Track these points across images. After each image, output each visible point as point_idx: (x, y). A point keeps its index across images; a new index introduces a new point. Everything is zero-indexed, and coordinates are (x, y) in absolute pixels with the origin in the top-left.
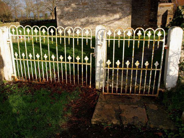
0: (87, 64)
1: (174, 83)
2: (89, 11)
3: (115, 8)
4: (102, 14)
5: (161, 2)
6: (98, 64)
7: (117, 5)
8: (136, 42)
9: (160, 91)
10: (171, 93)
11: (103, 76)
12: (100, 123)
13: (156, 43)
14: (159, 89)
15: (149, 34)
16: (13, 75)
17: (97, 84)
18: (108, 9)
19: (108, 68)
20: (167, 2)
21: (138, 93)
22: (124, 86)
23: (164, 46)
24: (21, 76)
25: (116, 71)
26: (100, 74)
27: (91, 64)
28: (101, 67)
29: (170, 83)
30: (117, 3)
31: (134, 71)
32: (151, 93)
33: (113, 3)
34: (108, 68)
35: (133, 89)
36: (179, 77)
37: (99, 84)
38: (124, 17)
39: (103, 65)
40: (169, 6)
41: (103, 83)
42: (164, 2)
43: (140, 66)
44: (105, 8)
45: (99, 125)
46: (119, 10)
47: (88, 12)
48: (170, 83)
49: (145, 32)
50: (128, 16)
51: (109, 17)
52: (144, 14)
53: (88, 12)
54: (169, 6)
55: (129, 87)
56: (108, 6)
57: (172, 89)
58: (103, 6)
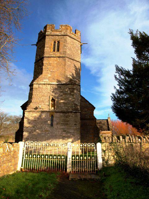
0: (63, 160)
1: (102, 165)
2: (50, 136)
3: (69, 135)
4: (60, 138)
5: (102, 130)
6: (68, 160)
7: (70, 133)
8: (84, 149)
9: (96, 171)
10: (100, 171)
11: (70, 166)
12: (73, 179)
13: (92, 149)
14: (95, 170)
15: (89, 146)
16: (22, 168)
17: (68, 170)
18: (64, 135)
19: (81, 148)
20: (106, 130)
21: (87, 172)
22: (80, 170)
23: (95, 150)
24: (26, 168)
25: (76, 161)
26: (69, 165)
27: (65, 160)
28: (70, 161)
29: (100, 167)
30: (70, 131)
31: (84, 161)
32: (92, 172)
33: (67, 131)
34: (81, 148)
35: (84, 170)
36: (103, 163)
37: (68, 170)
38: (75, 141)
39: (71, 160)
40: (109, 133)
41: (71, 169)
42: (105, 130)
43: (86, 159)
44: (61, 135)
45: (72, 179)
46: (71, 136)
47: (49, 137)
48: (100, 167)
49: (87, 145)
50: (78, 140)
51: (64, 141)
52: (90, 139)
53: (49, 137)
54: (109, 133)
55: (83, 170)
56: (64, 133)
57: (101, 169)
58: (60, 133)
